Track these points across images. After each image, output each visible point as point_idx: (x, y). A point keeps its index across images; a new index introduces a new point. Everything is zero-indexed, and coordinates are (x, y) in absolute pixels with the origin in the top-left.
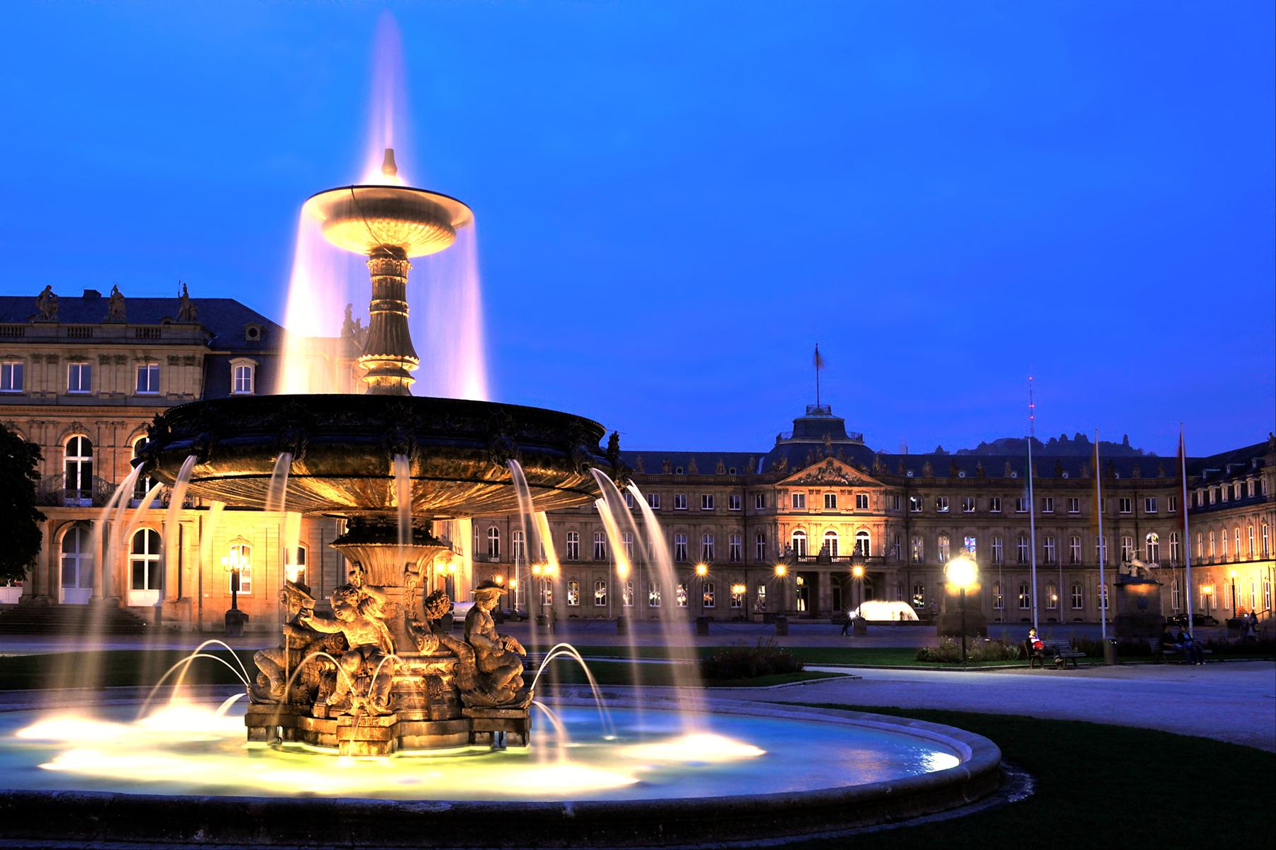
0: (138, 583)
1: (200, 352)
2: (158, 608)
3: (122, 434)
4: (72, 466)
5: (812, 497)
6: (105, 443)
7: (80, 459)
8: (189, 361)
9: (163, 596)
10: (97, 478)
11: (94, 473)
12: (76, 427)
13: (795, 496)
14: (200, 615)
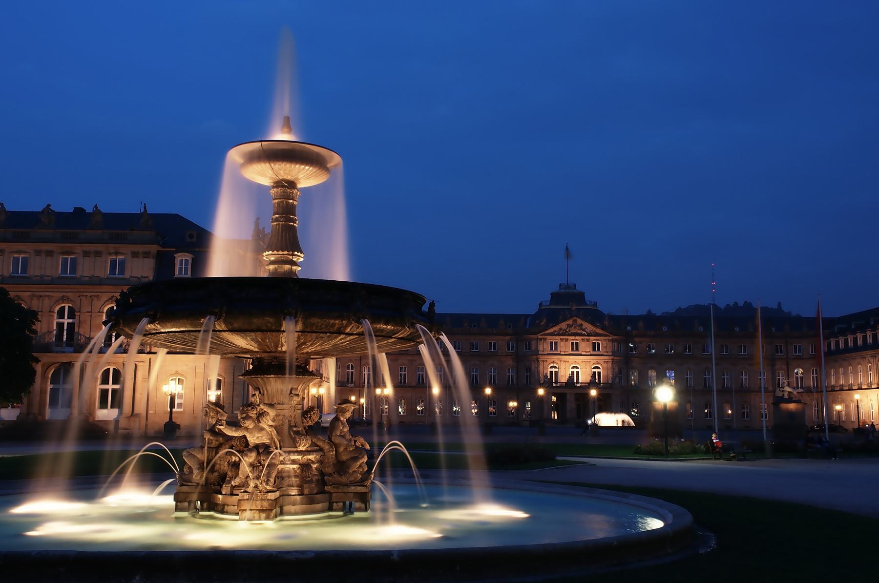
0: (103, 405)
1: (154, 248)
2: (117, 421)
3: (97, 304)
4: (60, 326)
5: (563, 343)
6: (86, 308)
7: (66, 321)
8: (146, 255)
9: (120, 413)
10: (78, 333)
11: (76, 330)
12: (63, 299)
13: (551, 343)
14: (146, 425)
